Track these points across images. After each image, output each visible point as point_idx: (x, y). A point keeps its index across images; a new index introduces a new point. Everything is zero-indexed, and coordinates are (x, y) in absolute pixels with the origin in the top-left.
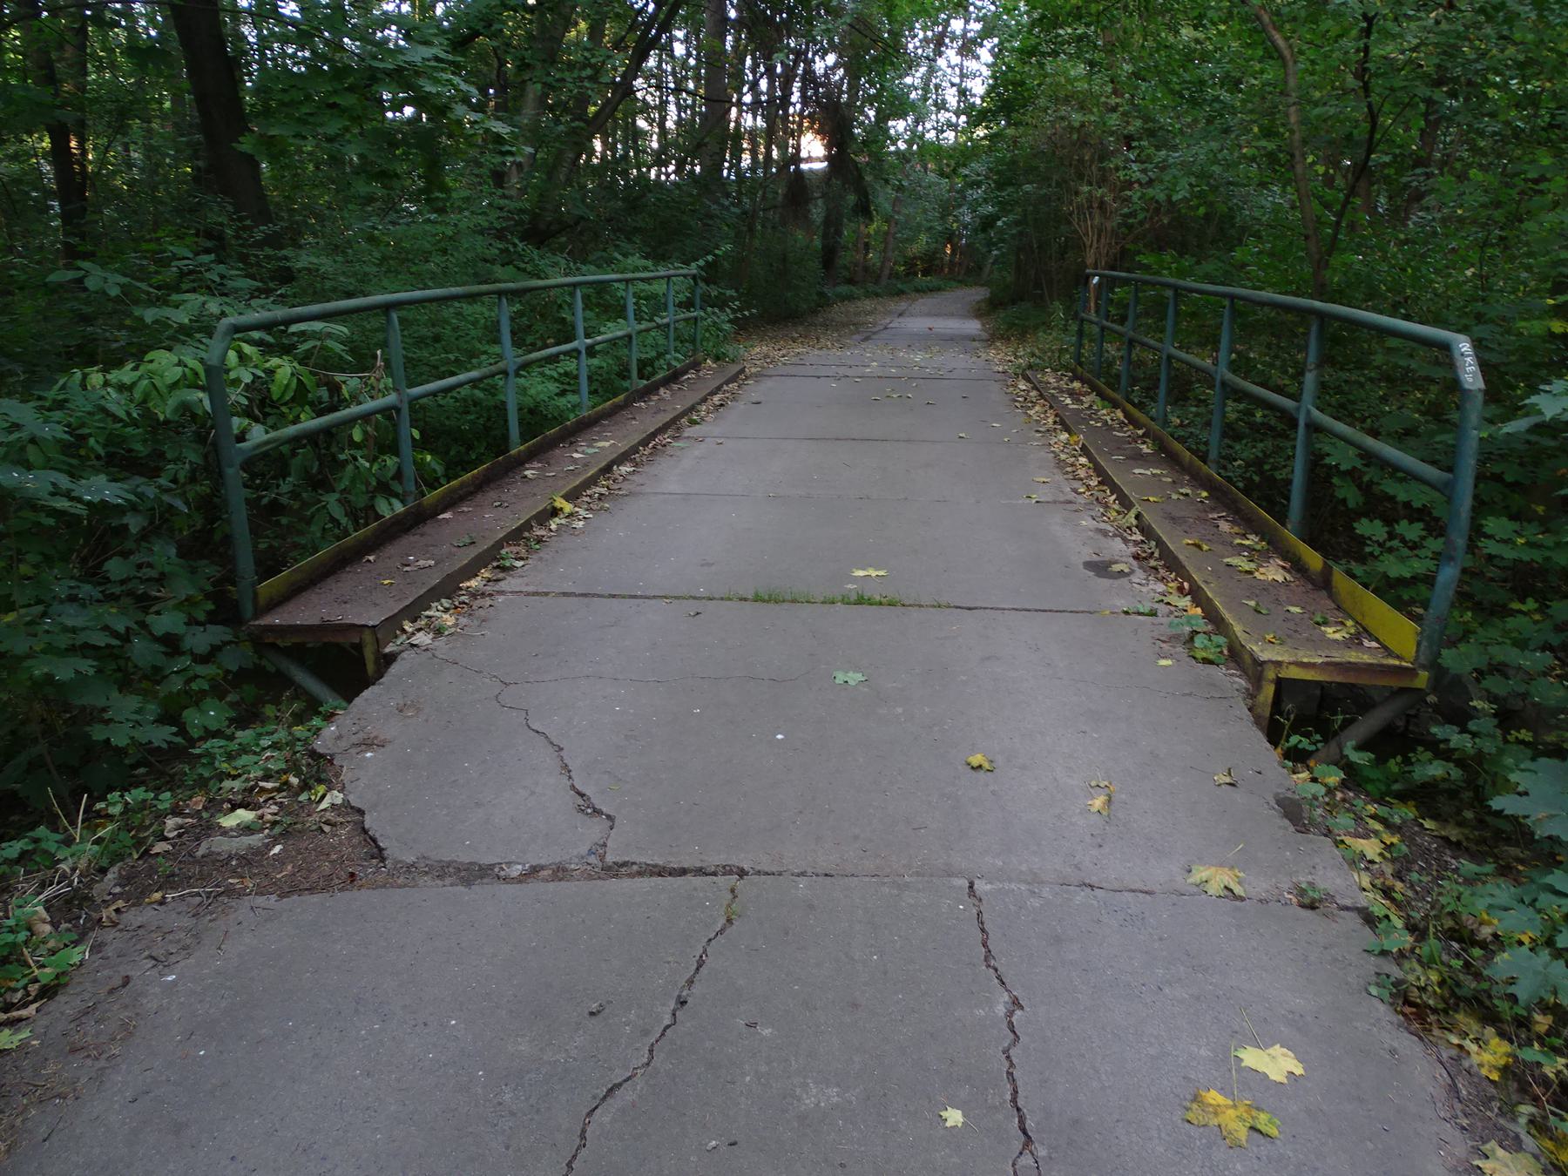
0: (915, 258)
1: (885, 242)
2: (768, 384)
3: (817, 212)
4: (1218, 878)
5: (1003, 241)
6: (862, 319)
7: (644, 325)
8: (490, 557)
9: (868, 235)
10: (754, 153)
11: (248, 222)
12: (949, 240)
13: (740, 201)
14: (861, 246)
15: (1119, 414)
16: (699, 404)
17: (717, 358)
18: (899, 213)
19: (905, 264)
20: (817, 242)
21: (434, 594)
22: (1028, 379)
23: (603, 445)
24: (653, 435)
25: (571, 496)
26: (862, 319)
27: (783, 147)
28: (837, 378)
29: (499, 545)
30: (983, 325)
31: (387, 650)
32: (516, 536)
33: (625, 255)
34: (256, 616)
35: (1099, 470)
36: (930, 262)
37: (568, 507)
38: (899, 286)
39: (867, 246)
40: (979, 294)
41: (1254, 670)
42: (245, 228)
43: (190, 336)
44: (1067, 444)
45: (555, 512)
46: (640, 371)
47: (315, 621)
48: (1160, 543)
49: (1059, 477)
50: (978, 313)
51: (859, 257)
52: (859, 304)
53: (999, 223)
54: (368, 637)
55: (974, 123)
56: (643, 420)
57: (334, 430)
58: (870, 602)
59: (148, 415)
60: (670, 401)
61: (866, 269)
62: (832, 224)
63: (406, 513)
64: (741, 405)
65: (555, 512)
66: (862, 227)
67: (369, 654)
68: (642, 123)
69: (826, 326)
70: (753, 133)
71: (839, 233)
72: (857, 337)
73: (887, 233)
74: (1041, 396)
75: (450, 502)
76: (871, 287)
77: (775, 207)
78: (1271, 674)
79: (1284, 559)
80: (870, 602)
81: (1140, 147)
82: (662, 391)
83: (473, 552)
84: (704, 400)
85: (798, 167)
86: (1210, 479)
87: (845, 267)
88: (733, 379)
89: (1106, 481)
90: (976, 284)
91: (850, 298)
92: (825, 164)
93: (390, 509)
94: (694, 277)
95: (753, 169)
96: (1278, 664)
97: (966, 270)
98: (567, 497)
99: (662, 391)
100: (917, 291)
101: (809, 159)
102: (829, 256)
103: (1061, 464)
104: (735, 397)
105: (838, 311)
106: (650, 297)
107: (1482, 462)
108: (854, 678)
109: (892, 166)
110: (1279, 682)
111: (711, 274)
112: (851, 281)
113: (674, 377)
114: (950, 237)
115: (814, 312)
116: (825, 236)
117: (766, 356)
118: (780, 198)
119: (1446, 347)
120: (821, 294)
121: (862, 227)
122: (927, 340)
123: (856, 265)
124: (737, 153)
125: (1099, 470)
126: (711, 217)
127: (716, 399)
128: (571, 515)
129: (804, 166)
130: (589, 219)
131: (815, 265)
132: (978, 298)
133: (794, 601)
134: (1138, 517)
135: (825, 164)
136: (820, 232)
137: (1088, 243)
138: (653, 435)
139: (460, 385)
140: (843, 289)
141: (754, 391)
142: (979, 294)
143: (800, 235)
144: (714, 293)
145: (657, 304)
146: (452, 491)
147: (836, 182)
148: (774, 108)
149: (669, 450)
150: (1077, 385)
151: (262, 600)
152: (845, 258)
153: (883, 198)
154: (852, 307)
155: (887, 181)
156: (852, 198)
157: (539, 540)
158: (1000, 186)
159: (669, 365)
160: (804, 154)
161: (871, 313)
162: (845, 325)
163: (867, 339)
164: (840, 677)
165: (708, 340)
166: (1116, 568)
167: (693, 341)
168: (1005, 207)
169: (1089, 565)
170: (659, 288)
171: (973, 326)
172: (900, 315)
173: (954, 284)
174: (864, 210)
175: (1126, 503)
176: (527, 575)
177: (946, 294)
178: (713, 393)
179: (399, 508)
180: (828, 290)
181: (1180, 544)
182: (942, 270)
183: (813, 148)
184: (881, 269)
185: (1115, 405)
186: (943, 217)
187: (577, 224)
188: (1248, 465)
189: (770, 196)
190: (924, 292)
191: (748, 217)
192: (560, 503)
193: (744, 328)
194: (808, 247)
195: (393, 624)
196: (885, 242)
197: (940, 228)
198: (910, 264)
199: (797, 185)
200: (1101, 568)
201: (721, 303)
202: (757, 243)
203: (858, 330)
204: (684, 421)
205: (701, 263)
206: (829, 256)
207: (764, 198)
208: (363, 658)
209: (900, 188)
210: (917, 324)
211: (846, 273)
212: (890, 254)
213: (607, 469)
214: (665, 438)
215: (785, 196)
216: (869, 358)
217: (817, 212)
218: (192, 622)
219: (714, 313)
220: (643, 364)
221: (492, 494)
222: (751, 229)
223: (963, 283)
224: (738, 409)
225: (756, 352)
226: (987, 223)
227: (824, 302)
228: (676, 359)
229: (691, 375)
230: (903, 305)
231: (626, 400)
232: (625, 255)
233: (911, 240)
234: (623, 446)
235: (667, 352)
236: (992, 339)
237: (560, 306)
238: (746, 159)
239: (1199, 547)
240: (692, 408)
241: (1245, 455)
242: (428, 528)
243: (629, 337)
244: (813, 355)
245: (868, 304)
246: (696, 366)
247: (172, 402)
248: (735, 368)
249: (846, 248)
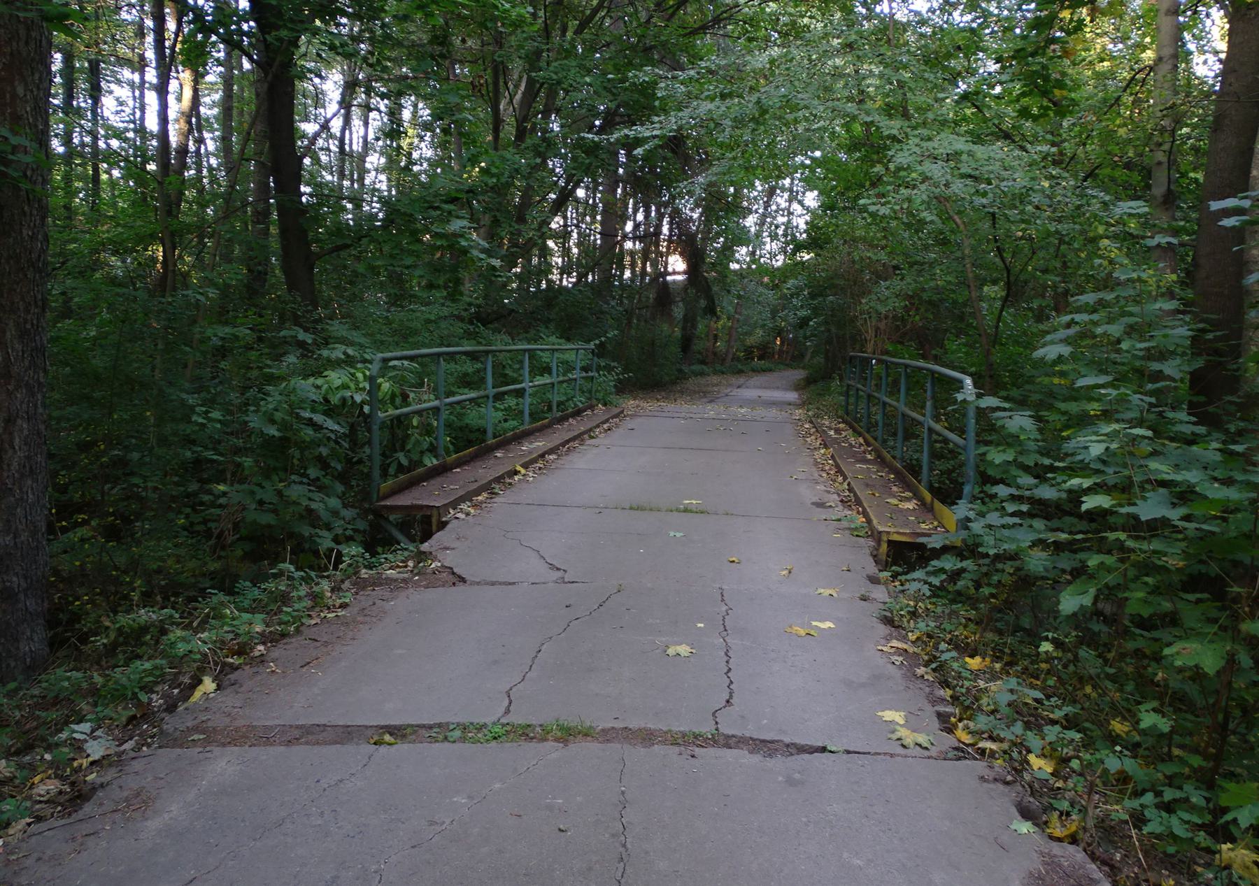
0: (752, 347)
1: (730, 334)
2: (639, 420)
3: (678, 311)
4: (826, 592)
5: (815, 336)
6: (710, 389)
7: (561, 378)
8: (487, 488)
9: (717, 329)
10: (633, 266)
11: (310, 308)
12: (779, 334)
13: (622, 302)
14: (711, 337)
15: (861, 440)
16: (595, 427)
17: (605, 405)
18: (740, 314)
19: (745, 351)
20: (678, 332)
21: (462, 499)
22: (811, 422)
23: (538, 444)
24: (568, 442)
25: (525, 466)
26: (710, 389)
27: (655, 264)
28: (684, 418)
29: (490, 482)
30: (800, 395)
31: (444, 519)
32: (498, 480)
33: (548, 337)
34: (377, 501)
35: (837, 466)
36: (764, 352)
37: (523, 471)
38: (740, 367)
39: (716, 337)
40: (799, 374)
41: (876, 536)
42: (307, 312)
43: (339, 365)
44: (824, 454)
45: (516, 473)
46: (558, 406)
47: (409, 503)
48: (855, 495)
49: (814, 469)
50: (797, 387)
51: (709, 344)
52: (709, 378)
53: (811, 323)
54: (435, 512)
55: (799, 247)
56: (560, 434)
57: (402, 419)
58: (691, 511)
59: (327, 400)
60: (575, 426)
61: (715, 354)
62: (689, 321)
63: (440, 465)
64: (621, 430)
65: (516, 473)
66: (712, 323)
67: (434, 520)
68: (551, 243)
69: (682, 393)
70: (632, 253)
71: (694, 326)
72: (705, 400)
73: (731, 328)
74: (817, 431)
75: (460, 463)
76: (718, 367)
77: (647, 307)
78: (885, 538)
79: (919, 500)
80: (691, 511)
81: (901, 274)
82: (571, 420)
83: (475, 486)
84: (598, 426)
85: (665, 279)
86: (896, 468)
87: (700, 353)
88: (616, 416)
89: (840, 471)
90: (799, 368)
91: (702, 374)
92: (685, 276)
93: (431, 461)
94: (593, 352)
95: (632, 279)
96: (888, 533)
97: (792, 357)
98: (522, 466)
99: (571, 420)
100: (753, 370)
101: (674, 273)
102: (686, 343)
103: (816, 463)
104: (617, 426)
105: (691, 383)
106: (566, 362)
107: (977, 435)
108: (699, 625)
109: (733, 281)
110: (890, 542)
111: (601, 351)
112: (703, 362)
113: (578, 413)
114: (779, 332)
115: (674, 383)
116: (684, 329)
117: (638, 406)
118: (651, 300)
119: (961, 382)
120: (680, 371)
121: (712, 323)
122: (752, 404)
123: (707, 350)
124: (622, 268)
125: (837, 466)
126: (602, 312)
127: (605, 426)
128: (524, 475)
129: (669, 278)
130: (517, 312)
131: (675, 349)
132: (799, 377)
133: (651, 510)
134: (849, 484)
135: (685, 276)
136: (680, 325)
137: (868, 338)
138: (568, 442)
139: (465, 401)
140: (696, 367)
141: (629, 423)
142: (799, 374)
143: (665, 327)
144: (603, 364)
145: (569, 367)
146: (459, 458)
147: (692, 291)
148: (649, 237)
149: (577, 450)
150: (842, 426)
151: (381, 494)
152: (698, 346)
153: (727, 304)
154: (702, 381)
155: (729, 292)
156: (703, 303)
157: (510, 484)
158: (813, 296)
159: (575, 405)
160: (670, 269)
161: (717, 385)
162: (695, 392)
163: (710, 402)
164: (672, 534)
165: (599, 391)
166: (828, 504)
167: (590, 392)
168: (816, 311)
169: (813, 504)
170: (570, 356)
171: (792, 396)
172: (739, 387)
173: (782, 367)
174: (711, 311)
175: (845, 478)
176: (503, 499)
177: (776, 374)
178: (604, 423)
179: (435, 462)
180: (686, 369)
181: (863, 494)
182: (773, 357)
183: (677, 264)
184: (727, 351)
185: (860, 435)
186: (773, 318)
187: (509, 314)
188: (942, 473)
189: (644, 299)
190: (759, 372)
191: (629, 313)
192: (519, 468)
193: (623, 388)
194: (670, 336)
195: (446, 507)
196: (730, 334)
197: (771, 325)
198: (749, 352)
199: (663, 291)
200: (821, 505)
201: (609, 369)
202: (633, 332)
203: (705, 395)
204: (586, 436)
205: (597, 342)
206: (686, 343)
207: (640, 300)
208: (431, 522)
209: (739, 297)
210: (750, 393)
211: (699, 356)
212: (732, 343)
213: (542, 456)
214: (576, 444)
215: (655, 299)
216: (711, 411)
217: (678, 311)
218: (345, 506)
219: (604, 375)
220: (559, 404)
221: (478, 464)
222: (629, 322)
223: (789, 366)
224: (617, 434)
225: (630, 404)
226: (804, 323)
227: (681, 376)
228: (580, 401)
229: (589, 412)
230: (742, 380)
231: (550, 422)
232: (548, 337)
233: (749, 334)
234: (550, 445)
235: (574, 397)
236: (802, 405)
237: (504, 367)
238: (627, 274)
239: (874, 494)
240: (591, 430)
241: (941, 468)
242: (449, 474)
243: (553, 384)
244: (670, 407)
245: (715, 379)
246: (592, 407)
247: (339, 396)
248: (616, 411)
249: (700, 338)
